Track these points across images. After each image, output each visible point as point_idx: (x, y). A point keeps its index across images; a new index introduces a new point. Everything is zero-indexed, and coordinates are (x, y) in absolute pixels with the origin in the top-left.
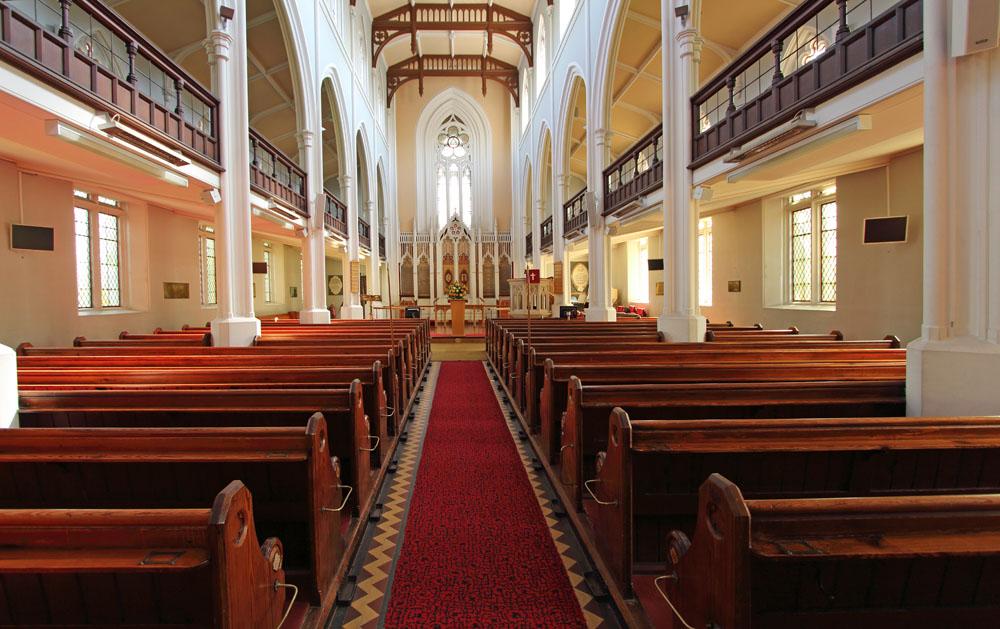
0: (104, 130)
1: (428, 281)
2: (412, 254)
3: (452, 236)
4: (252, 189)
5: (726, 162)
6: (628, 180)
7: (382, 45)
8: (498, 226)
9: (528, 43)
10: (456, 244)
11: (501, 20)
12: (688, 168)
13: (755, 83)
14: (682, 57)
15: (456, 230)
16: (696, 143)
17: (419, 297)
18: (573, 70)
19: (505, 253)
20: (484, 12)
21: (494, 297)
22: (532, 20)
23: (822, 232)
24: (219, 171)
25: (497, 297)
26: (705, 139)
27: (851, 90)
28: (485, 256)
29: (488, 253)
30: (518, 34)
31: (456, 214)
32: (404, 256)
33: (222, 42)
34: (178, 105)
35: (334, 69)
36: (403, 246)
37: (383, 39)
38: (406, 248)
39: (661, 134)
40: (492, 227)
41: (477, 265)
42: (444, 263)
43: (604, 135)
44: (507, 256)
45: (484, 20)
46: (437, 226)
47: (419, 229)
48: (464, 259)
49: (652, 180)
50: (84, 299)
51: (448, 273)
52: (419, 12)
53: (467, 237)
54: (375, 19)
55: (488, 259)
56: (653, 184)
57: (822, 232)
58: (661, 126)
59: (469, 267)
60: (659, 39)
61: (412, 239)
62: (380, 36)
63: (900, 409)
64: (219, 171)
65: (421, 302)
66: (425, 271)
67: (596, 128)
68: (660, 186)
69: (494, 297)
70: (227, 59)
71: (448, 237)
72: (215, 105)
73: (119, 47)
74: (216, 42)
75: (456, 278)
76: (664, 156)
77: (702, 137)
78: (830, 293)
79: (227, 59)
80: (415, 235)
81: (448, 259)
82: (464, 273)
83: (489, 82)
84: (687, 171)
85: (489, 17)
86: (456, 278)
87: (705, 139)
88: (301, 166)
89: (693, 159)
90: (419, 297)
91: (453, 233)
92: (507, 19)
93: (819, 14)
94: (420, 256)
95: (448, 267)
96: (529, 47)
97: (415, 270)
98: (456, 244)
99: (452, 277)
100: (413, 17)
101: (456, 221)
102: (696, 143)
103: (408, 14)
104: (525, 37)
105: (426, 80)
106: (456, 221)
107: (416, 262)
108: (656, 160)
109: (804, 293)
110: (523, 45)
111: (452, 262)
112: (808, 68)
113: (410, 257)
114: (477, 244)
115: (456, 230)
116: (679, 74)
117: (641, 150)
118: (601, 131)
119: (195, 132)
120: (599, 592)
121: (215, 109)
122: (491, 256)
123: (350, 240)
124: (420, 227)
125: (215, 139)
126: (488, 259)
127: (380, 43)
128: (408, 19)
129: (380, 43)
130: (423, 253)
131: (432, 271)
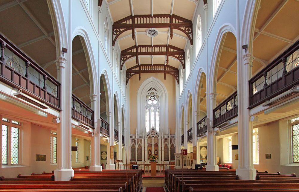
1: (142, 154)
2: (135, 143)
3: (151, 136)
5: (264, 106)
8: (170, 132)
9: (183, 60)
10: (153, 139)
12: (213, 127)
13: (275, 75)
14: (245, 64)
16: (251, 98)
17: (138, 161)
18: (201, 70)
19: (173, 143)
21: (168, 160)
23: (293, 136)
24: (60, 111)
25: (170, 161)
26: (231, 112)
27: (258, 106)
28: (165, 144)
29: (166, 143)
31: (153, 127)
32: (132, 144)
34: (45, 86)
35: (105, 71)
36: (132, 140)
39: (237, 95)
41: (161, 147)
42: (148, 147)
44: (174, 144)
46: (146, 132)
48: (156, 145)
49: (233, 114)
50: (4, 161)
51: (150, 151)
53: (157, 136)
55: (166, 145)
56: (234, 115)
59: (158, 148)
60: (236, 58)
61: (135, 137)
64: (60, 111)
65: (139, 163)
66: (140, 150)
67: (210, 93)
68: (237, 116)
69: (168, 160)
70: (64, 68)
72: (59, 85)
73: (23, 64)
75: (153, 153)
76: (238, 104)
80: (137, 135)
81: (150, 145)
82: (156, 150)
84: (248, 110)
86: (153, 153)
89: (250, 105)
90: (138, 161)
91: (152, 134)
94: (138, 144)
95: (150, 148)
97: (136, 150)
98: (153, 139)
99: (151, 152)
101: (153, 130)
102: (251, 98)
105: (141, 74)
106: (153, 130)
107: (137, 146)
111: (151, 147)
112: (274, 83)
114: (161, 140)
116: (244, 71)
119: (51, 96)
121: (59, 87)
122: (167, 144)
124: (138, 132)
125: (58, 99)
126: (166, 145)
127: (124, 60)
128: (131, 23)
130: (140, 143)
131: (143, 150)
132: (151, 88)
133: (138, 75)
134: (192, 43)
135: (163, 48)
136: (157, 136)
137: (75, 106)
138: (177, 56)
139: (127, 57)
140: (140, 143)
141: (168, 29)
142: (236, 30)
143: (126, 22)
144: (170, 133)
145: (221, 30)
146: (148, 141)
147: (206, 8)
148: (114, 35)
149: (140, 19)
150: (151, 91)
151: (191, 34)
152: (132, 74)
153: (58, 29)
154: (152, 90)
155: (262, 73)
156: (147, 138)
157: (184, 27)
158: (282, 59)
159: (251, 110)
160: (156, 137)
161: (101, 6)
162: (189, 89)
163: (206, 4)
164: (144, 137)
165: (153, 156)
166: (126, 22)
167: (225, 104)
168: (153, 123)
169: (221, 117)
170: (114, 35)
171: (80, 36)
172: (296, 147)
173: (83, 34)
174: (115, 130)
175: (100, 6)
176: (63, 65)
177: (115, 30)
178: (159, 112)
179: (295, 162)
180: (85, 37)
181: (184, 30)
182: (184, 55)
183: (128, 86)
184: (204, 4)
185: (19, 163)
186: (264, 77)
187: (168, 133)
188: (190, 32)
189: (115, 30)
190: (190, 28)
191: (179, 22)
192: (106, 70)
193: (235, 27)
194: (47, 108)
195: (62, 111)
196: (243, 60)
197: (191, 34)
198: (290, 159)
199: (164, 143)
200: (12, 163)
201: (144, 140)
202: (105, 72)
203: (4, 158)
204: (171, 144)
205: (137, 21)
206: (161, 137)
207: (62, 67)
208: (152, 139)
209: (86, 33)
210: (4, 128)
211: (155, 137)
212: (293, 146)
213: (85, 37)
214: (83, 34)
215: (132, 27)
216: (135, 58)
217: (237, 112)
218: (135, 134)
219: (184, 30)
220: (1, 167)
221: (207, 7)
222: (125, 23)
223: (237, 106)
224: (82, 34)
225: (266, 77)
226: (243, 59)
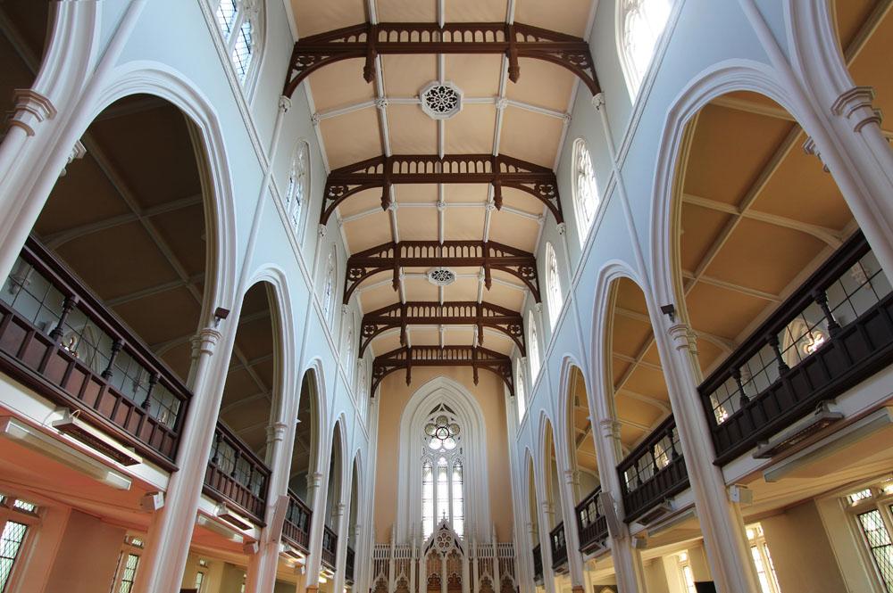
2: (387, 573)
3: (439, 550)
6: (648, 478)
8: (497, 536)
9: (519, 335)
10: (445, 560)
12: (714, 464)
15: (444, 541)
16: (715, 435)
18: (568, 360)
19: (507, 573)
20: (474, 309)
24: (170, 470)
28: (482, 578)
29: (486, 574)
30: (520, 269)
31: (444, 520)
33: (211, 338)
35: (318, 360)
36: (377, 564)
37: (359, 276)
38: (380, 566)
40: (489, 537)
43: (611, 425)
45: (474, 315)
46: (422, 536)
47: (398, 541)
49: (675, 478)
57: (871, 549)
62: (369, 330)
64: (170, 470)
68: (687, 485)
71: (434, 551)
73: (103, 344)
76: (683, 449)
83: (506, 191)
88: (266, 463)
93: (761, 351)
94: (398, 579)
98: (445, 560)
101: (444, 529)
102: (715, 435)
103: (399, 311)
105: (393, 188)
106: (444, 529)
108: (675, 454)
113: (385, 579)
115: (444, 541)
121: (186, 402)
122: (490, 578)
124: (400, 537)
128: (404, 358)
130: (402, 574)
132: (439, 405)
136: (459, 551)
140: (402, 574)
144: (498, 541)
146: (428, 568)
150: (438, 414)
154: (442, 410)
155: (762, 339)
156: (426, 558)
159: (723, 468)
160: (454, 551)
164: (418, 553)
168: (443, 507)
170: (348, 281)
176: (210, 347)
178: (461, 473)
183: (376, 401)
186: (668, 439)
187: (492, 541)
193: (637, 271)
194: (135, 462)
199: (480, 573)
201: (417, 561)
202: (316, 363)
204: (503, 577)
206: (470, 552)
208: (441, 561)
209: (282, 276)
211: (449, 555)
215: (395, 264)
216: (398, 331)
218: (390, 542)
219: (517, 270)
224: (271, 278)
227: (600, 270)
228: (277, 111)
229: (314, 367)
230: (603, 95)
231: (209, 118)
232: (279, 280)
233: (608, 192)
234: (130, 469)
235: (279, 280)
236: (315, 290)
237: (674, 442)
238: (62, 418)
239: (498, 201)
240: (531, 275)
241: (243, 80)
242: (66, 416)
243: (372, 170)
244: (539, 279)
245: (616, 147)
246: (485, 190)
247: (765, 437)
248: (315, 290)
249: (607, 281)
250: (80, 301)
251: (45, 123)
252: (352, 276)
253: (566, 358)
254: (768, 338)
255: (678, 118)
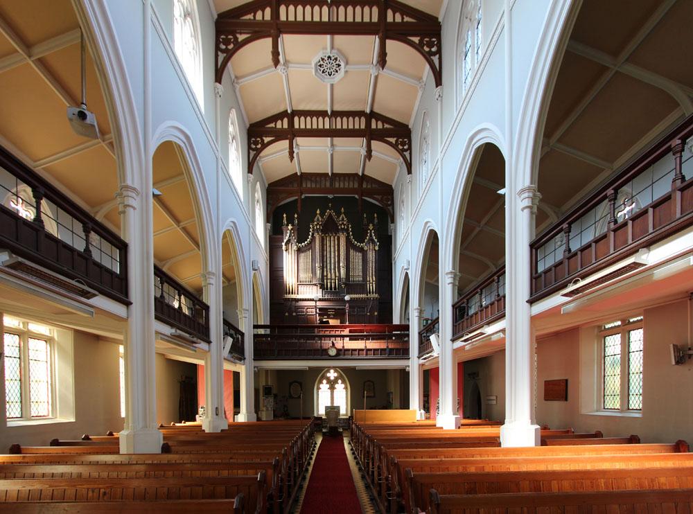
0: (8, 266)
4: (157, 318)
5: (565, 295)
7: (259, 151)
9: (406, 150)
11: (369, 186)
12: (527, 302)
14: (523, 210)
16: (534, 280)
18: (428, 225)
20: (363, 119)
22: (393, 187)
24: (128, 304)
30: (397, 141)
34: (162, 293)
35: (234, 223)
37: (231, 47)
39: (504, 272)
43: (453, 276)
45: (363, 126)
50: (13, 410)
52: (296, 119)
54: (251, 125)
56: (497, 314)
58: (438, 318)
62: (227, 42)
63: (499, 445)
64: (128, 304)
68: (503, 316)
70: (134, 208)
72: (123, 247)
73: (78, 227)
74: (125, 193)
77: (540, 276)
78: (636, 402)
79: (134, 208)
83: (394, 47)
84: (451, 342)
85: (368, 124)
87: (543, 276)
89: (453, 335)
92: (407, 19)
96: (435, 59)
100: (291, 123)
102: (534, 280)
103: (286, 120)
104: (430, 45)
105: (299, 140)
109: (614, 403)
110: (401, 152)
117: (484, 288)
118: (418, 309)
120: (371, 494)
123: (133, 307)
127: (256, 149)
128: (286, 126)
129: (256, 149)
133: (269, 41)
134: (410, 172)
135: (357, 119)
137: (165, 294)
138: (393, 140)
139: (265, 142)
141: (374, 41)
142: (504, 137)
143: (254, 16)
145: (472, 139)
147: (439, 96)
148: (251, 151)
149: (306, 119)
151: (438, 56)
152: (267, 140)
153: (115, 103)
157: (394, 137)
158: (606, 194)
161: (220, 83)
162: (430, 220)
163: (439, 87)
165: (380, 480)
166: (254, 16)
167: (477, 293)
169: (469, 320)
170: (251, 151)
171: (175, 143)
172: (612, 379)
173: (179, 139)
174: (226, 322)
175: (217, 84)
176: (212, 281)
177: (222, 37)
179: (633, 409)
180: (186, 147)
181: (394, 142)
182: (410, 137)
184: (437, 87)
185: (24, 415)
188: (406, 147)
189: (253, 139)
190: (434, 39)
191: (405, 20)
192: (236, 221)
193: (504, 134)
194: (94, 295)
195: (131, 304)
196: (519, 201)
197: (438, 56)
198: (599, 402)
200: (33, 414)
202: (232, 225)
203: (14, 403)
205: (299, 123)
207: (129, 206)
209: (187, 137)
210: (10, 342)
212: (605, 376)
213: (186, 147)
214: (179, 139)
215: (291, 134)
216: (285, 143)
217: (505, 308)
219: (394, 142)
220: (6, 424)
221: (442, 93)
222: (252, 18)
223: (504, 297)
224: (177, 139)
225: (569, 236)
226: (517, 196)
227: (469, 137)
228: (214, 97)
229: (231, 228)
230: (442, 88)
231: (186, 138)
232: (185, 140)
233: (475, 80)
234: (93, 301)
235: (185, 140)
236: (220, 155)
237: (616, 207)
238: (8, 258)
239: (382, 60)
240: (434, 49)
241: (242, 200)
242: (10, 256)
243: (279, 125)
244: (443, 56)
245: (443, 135)
246: (371, 42)
247: (564, 286)
248: (220, 155)
249: (472, 148)
250: (45, 192)
251: (138, 199)
252: (254, 147)
253: (427, 223)
254: (564, 227)
255: (473, 143)
